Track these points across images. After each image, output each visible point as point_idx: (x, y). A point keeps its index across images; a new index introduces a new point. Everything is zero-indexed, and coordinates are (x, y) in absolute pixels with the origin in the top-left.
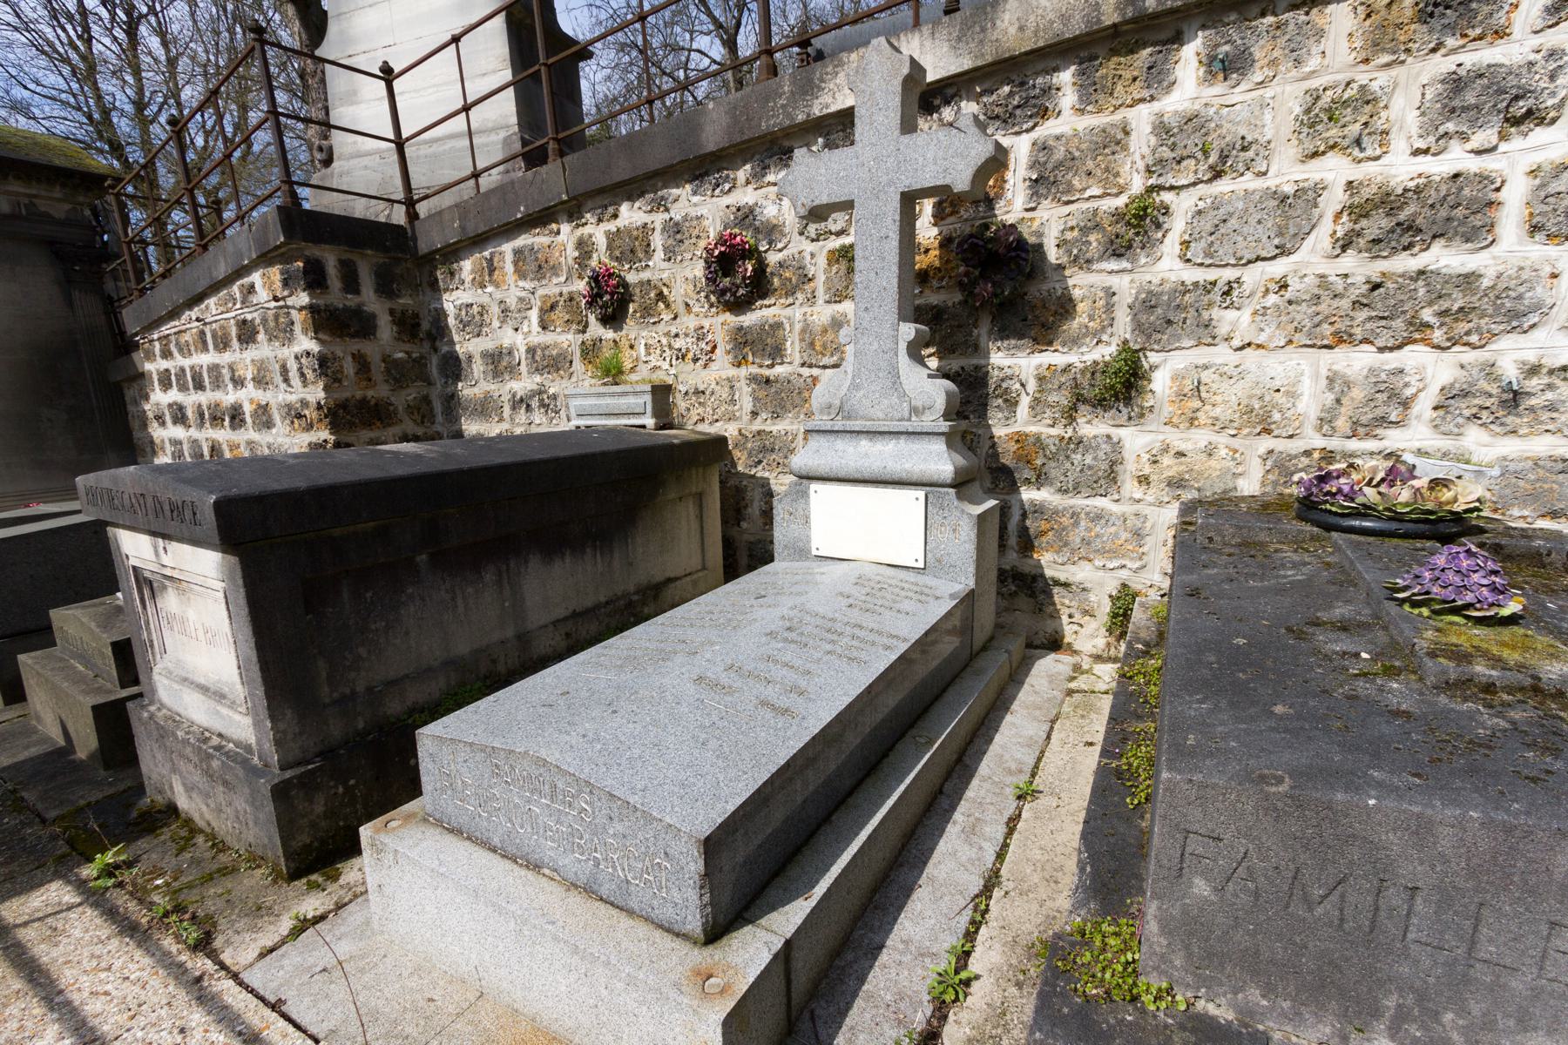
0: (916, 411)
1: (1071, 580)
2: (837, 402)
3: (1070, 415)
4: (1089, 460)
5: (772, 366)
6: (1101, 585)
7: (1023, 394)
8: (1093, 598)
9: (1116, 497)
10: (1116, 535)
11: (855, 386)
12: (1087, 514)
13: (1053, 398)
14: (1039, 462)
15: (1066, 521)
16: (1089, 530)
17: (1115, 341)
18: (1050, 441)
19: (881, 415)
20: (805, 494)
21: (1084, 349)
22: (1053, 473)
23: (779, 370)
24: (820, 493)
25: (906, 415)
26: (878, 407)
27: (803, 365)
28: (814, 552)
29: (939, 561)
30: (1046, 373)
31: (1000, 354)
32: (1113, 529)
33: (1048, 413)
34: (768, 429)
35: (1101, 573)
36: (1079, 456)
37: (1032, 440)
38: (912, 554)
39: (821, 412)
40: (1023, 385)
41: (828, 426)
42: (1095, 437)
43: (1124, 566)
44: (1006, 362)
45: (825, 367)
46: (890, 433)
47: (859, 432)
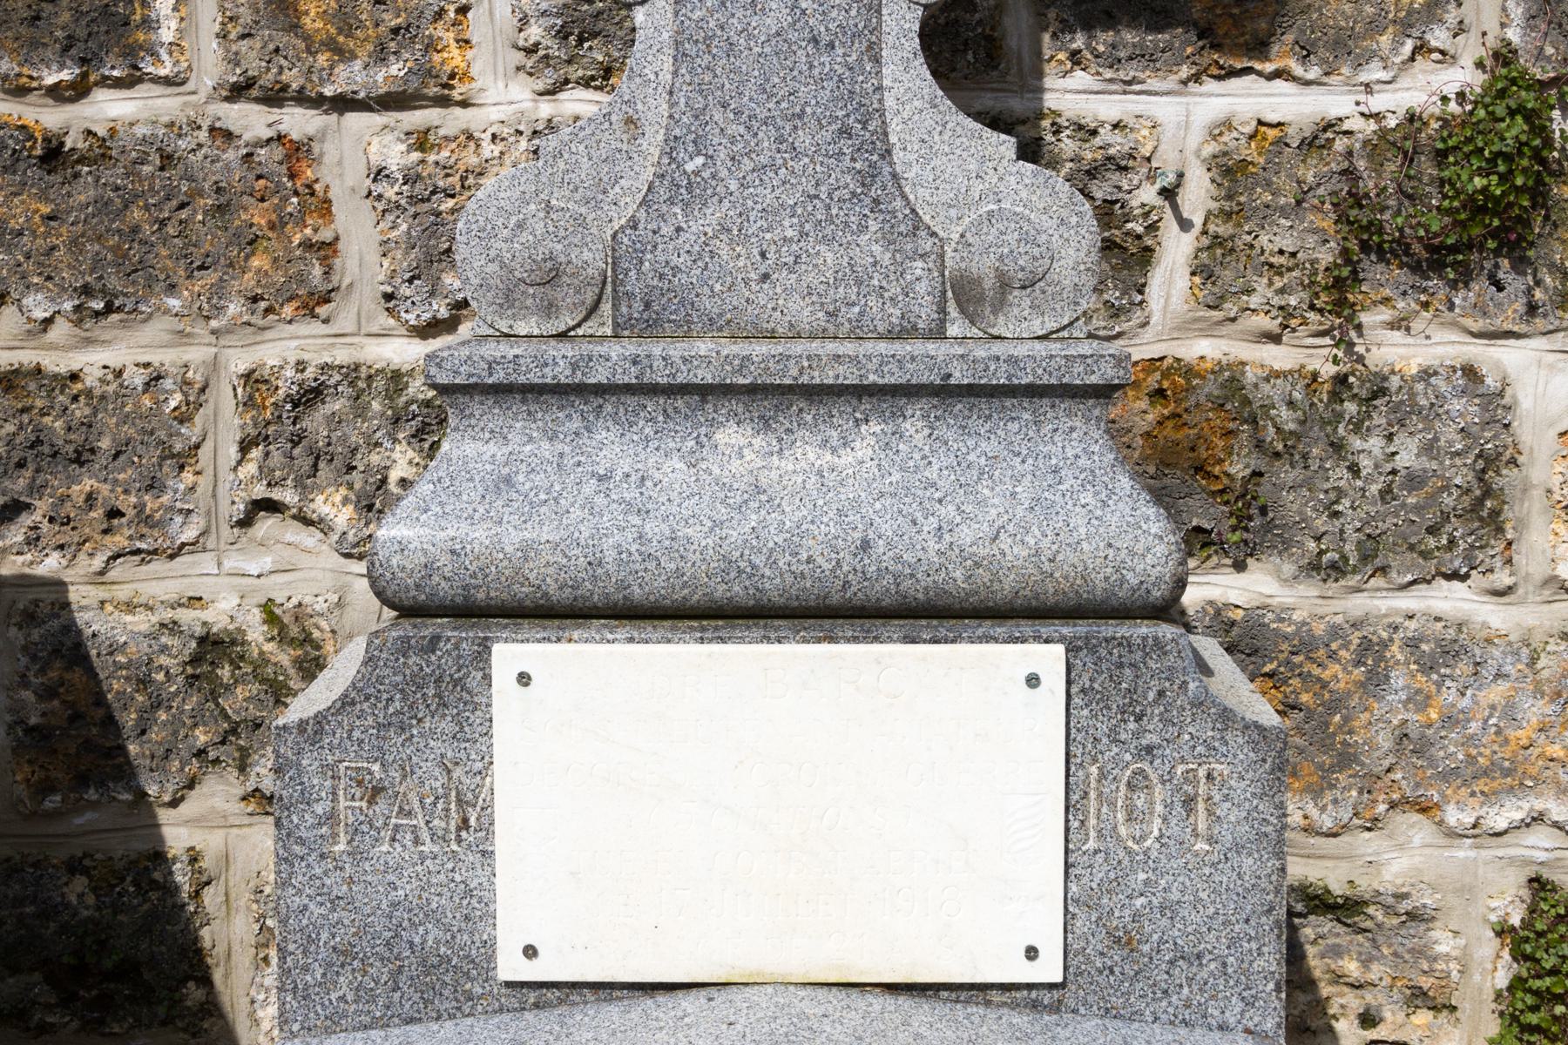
0: (966, 294)
1: (1366, 885)
2: (592, 258)
3: (1338, 296)
4: (1408, 456)
5: (78, 91)
6: (1467, 892)
7: (1170, 226)
8: (1444, 943)
9: (1503, 578)
10: (1509, 711)
11: (677, 188)
12: (1412, 644)
13: (1277, 239)
14: (1238, 468)
15: (1341, 675)
16: (1420, 700)
17: (1470, 50)
18: (1274, 392)
19: (805, 313)
20: (459, 697)
21: (1373, 72)
22: (1293, 504)
23: (109, 108)
24: (543, 691)
25: (925, 313)
26: (787, 279)
27: (238, 92)
28: (512, 966)
29: (1125, 942)
30: (1250, 152)
31: (1080, 78)
32: (1496, 693)
33: (1263, 292)
34: (57, 363)
35: (1464, 852)
36: (1375, 443)
37: (1211, 388)
38: (1011, 920)
39: (508, 300)
40: (1169, 194)
41: (559, 364)
42: (1427, 374)
43: (1539, 818)
44: (1108, 108)
45: (344, 104)
46: (861, 391)
47: (704, 392)
